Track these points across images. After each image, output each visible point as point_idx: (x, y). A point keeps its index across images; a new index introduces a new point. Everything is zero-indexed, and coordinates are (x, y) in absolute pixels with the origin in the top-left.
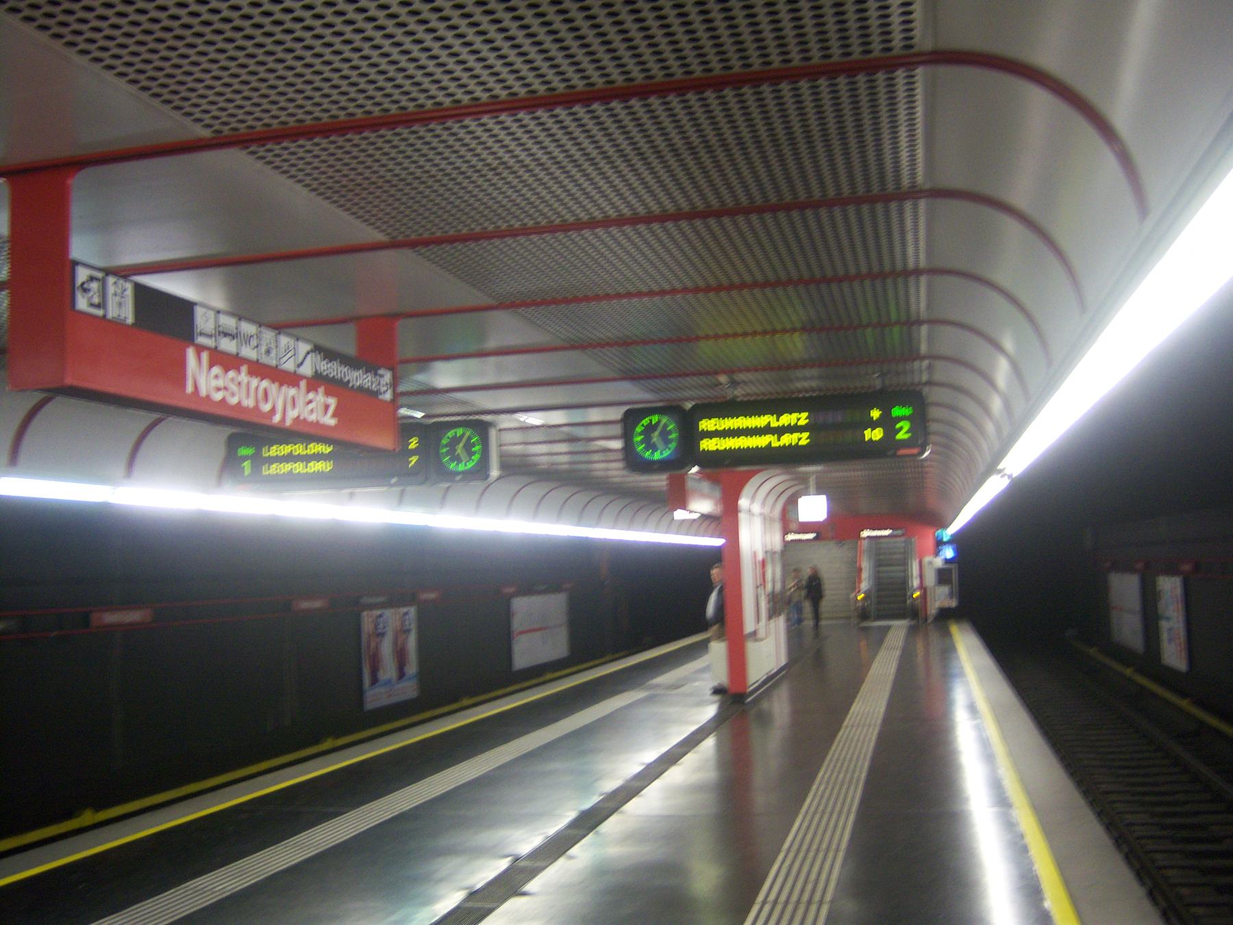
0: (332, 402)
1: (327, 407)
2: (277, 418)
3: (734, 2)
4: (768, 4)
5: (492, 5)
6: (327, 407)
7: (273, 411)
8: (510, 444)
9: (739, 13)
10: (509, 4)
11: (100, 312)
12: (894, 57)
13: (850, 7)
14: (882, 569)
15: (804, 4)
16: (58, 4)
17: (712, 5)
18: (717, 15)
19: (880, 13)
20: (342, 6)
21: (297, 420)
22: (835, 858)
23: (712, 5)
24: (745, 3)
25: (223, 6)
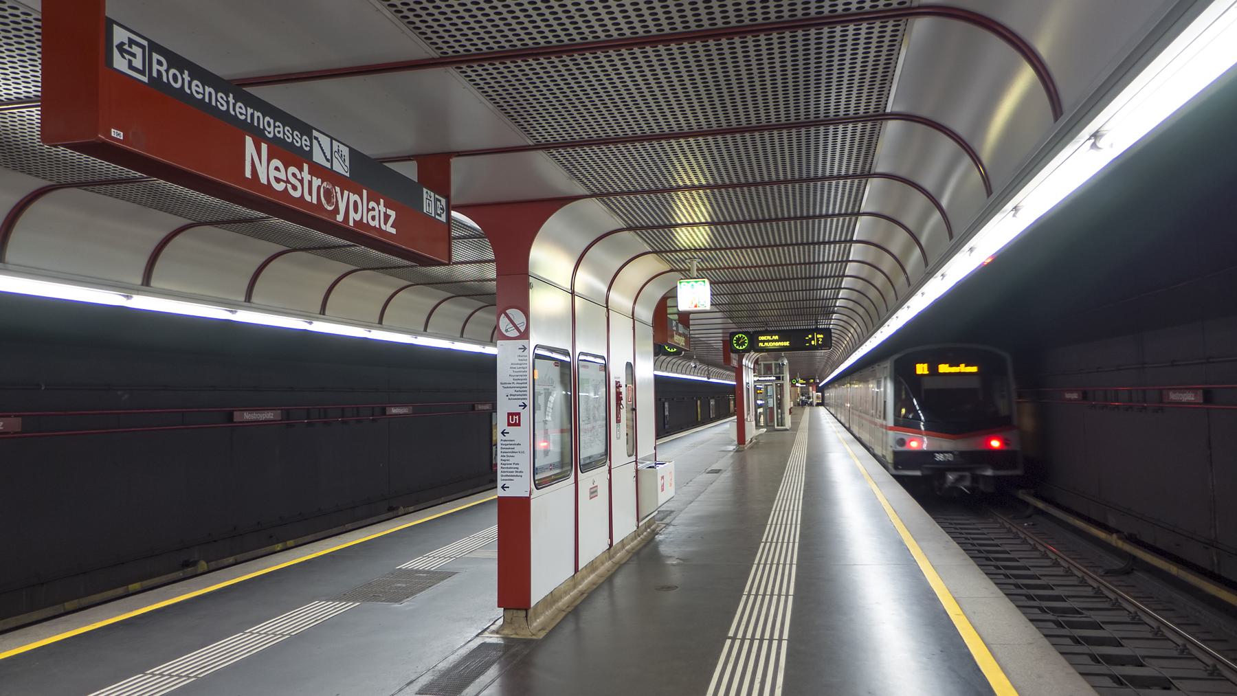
0: (392, 214)
1: (387, 217)
2: (340, 218)
3: (611, 2)
4: (804, 3)
5: (495, 3)
6: (387, 217)
7: (336, 211)
8: (464, 237)
9: (673, 9)
10: (607, 4)
11: (328, 165)
12: (691, 32)
13: (701, 5)
14: (115, 194)
15: (715, 3)
16: (5, 3)
17: (656, 4)
18: (659, 11)
19: (754, 11)
20: (426, 4)
21: (358, 223)
22: (786, 602)
23: (656, 4)
24: (618, 3)
25: (455, 3)
